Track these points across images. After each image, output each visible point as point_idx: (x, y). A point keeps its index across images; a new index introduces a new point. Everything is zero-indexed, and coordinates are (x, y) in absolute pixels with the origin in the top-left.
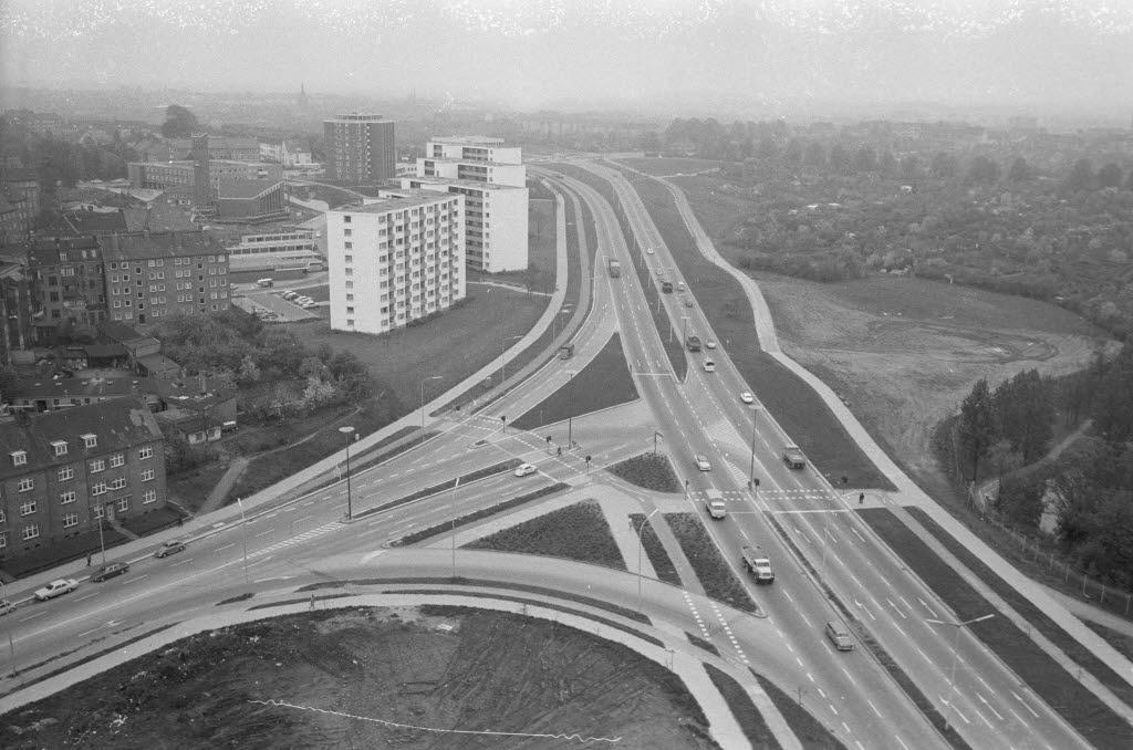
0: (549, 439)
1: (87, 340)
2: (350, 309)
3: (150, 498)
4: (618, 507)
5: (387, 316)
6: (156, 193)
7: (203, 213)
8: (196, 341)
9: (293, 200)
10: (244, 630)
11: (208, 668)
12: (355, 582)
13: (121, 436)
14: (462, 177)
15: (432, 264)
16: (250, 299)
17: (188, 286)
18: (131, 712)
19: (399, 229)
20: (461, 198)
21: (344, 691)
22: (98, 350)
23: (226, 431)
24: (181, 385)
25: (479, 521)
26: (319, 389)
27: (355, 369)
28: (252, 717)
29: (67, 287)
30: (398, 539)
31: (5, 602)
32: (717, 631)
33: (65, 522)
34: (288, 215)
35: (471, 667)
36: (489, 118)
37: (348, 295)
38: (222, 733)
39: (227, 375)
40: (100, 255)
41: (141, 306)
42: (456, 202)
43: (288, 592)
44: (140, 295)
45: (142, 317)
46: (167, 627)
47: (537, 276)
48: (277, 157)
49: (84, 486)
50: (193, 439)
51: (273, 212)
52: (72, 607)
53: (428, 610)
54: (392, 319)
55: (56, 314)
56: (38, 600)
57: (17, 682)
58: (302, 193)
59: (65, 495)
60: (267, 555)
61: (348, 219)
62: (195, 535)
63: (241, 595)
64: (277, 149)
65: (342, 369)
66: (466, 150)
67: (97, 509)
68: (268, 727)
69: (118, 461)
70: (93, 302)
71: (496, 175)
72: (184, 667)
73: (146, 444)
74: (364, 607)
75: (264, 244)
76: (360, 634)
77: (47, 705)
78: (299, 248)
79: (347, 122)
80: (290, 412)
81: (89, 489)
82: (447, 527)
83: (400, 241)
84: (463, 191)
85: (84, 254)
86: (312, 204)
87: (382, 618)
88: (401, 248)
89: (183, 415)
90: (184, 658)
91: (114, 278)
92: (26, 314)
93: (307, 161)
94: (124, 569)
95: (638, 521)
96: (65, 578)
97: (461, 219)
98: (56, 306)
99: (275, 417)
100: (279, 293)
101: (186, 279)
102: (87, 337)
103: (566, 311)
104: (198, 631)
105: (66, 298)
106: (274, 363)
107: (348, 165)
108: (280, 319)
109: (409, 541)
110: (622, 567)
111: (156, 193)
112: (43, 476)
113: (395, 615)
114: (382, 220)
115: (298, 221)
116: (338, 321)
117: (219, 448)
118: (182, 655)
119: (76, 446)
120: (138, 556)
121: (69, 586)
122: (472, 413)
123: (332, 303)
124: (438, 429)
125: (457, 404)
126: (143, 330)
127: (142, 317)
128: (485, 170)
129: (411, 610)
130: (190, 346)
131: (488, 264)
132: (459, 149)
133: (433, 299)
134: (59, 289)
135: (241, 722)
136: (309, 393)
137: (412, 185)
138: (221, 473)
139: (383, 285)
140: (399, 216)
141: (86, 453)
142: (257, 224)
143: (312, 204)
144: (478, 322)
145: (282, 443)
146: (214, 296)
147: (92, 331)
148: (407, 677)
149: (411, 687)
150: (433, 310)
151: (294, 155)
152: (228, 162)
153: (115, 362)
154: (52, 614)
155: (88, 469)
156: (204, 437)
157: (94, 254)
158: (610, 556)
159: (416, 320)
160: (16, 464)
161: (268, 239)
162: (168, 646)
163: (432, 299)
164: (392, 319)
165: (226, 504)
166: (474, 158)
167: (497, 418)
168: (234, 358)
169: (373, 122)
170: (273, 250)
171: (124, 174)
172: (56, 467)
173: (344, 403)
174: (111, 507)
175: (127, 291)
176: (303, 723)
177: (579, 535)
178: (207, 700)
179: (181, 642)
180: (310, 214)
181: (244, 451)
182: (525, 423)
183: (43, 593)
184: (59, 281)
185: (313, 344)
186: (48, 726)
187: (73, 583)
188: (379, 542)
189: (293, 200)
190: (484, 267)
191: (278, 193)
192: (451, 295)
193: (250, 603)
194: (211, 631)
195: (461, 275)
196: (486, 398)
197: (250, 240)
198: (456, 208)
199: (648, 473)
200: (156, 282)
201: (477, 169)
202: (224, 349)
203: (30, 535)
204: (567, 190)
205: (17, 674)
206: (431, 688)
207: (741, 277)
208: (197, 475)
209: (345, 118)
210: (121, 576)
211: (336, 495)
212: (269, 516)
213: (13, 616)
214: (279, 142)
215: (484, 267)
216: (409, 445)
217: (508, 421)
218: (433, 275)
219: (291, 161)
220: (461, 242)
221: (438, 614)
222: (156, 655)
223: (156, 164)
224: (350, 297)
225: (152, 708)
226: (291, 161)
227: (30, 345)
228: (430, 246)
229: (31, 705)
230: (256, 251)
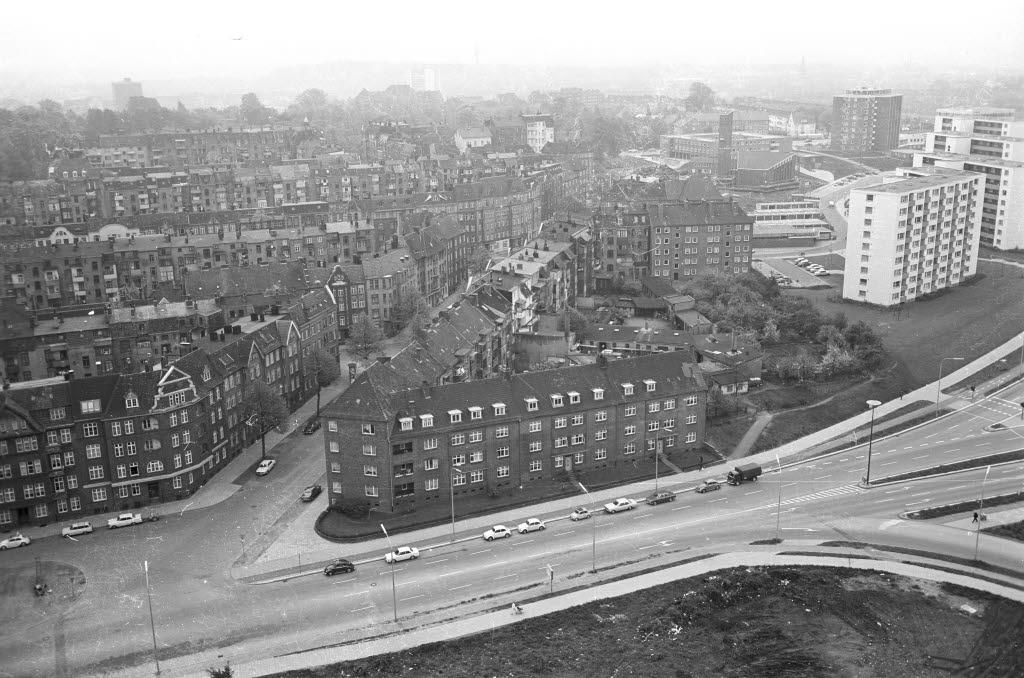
1: (633, 293)
2: (864, 281)
5: (899, 290)
6: (683, 162)
7: (723, 181)
8: (725, 302)
9: (803, 170)
10: (777, 572)
11: (747, 600)
12: (875, 547)
13: (675, 383)
14: (973, 152)
15: (946, 241)
16: (768, 263)
17: (717, 250)
18: (684, 625)
20: (982, 177)
21: (870, 649)
22: (643, 302)
23: (752, 385)
24: (714, 341)
25: (998, 507)
26: (837, 355)
27: (870, 339)
28: (786, 654)
29: (620, 247)
30: (916, 511)
31: (585, 509)
34: (798, 184)
35: (998, 655)
36: (990, 84)
37: (863, 268)
38: (761, 661)
39: (751, 334)
40: (647, 221)
42: (976, 181)
43: (812, 544)
45: (676, 275)
46: (710, 556)
48: (783, 128)
49: (643, 422)
50: (724, 390)
51: (785, 180)
52: (631, 522)
53: (949, 588)
54: (903, 292)
55: (610, 268)
57: (595, 578)
58: (809, 163)
59: (627, 428)
60: (792, 506)
61: (870, 198)
63: (771, 539)
64: (784, 120)
65: (857, 338)
66: (977, 124)
67: (651, 443)
68: (801, 666)
69: (670, 404)
70: (639, 260)
72: (726, 595)
74: (885, 573)
75: (775, 212)
76: (879, 595)
77: (620, 603)
78: (808, 217)
79: (857, 96)
80: (806, 374)
81: (646, 424)
83: (918, 220)
86: (818, 174)
87: (903, 586)
89: (718, 369)
90: (726, 587)
91: (658, 241)
92: (590, 268)
93: (811, 132)
94: (672, 498)
96: (627, 497)
97: (979, 199)
98: (610, 261)
99: (796, 379)
100: (792, 260)
101: (714, 244)
102: (633, 290)
104: (736, 565)
105: (619, 255)
106: (793, 326)
108: (794, 284)
109: (927, 515)
111: (683, 162)
112: (613, 411)
113: (916, 587)
114: (904, 199)
115: (804, 190)
116: (850, 291)
117: (746, 401)
118: (725, 584)
119: (640, 388)
120: (680, 488)
121: (412, 554)
122: (987, 394)
123: (847, 272)
124: (951, 406)
125: (970, 383)
126: (680, 287)
127: (676, 275)
128: (1000, 145)
129: (933, 585)
130: (720, 306)
131: (999, 241)
133: (944, 275)
134: (614, 247)
135: (777, 655)
136: (827, 359)
137: (925, 160)
138: (748, 425)
139: (899, 260)
140: (920, 196)
141: (648, 396)
142: (768, 192)
143: (818, 174)
145: (803, 403)
146: (737, 260)
147: (637, 285)
148: (930, 649)
149: (936, 661)
150: (943, 286)
151: (800, 126)
152: (744, 134)
153: (656, 314)
154: (618, 526)
155: (647, 409)
156: (734, 390)
157: (643, 219)
159: (925, 295)
160: (596, 398)
161: (779, 207)
162: (711, 573)
163: (944, 275)
164: (903, 292)
165: (753, 453)
166: (991, 132)
168: (758, 319)
170: (784, 217)
171: (656, 145)
172: (623, 405)
173: (858, 372)
176: (832, 671)
178: (746, 628)
179: (721, 572)
180: (817, 184)
181: (768, 407)
183: (611, 507)
184: (615, 241)
185: (827, 311)
186: (621, 621)
187: (633, 502)
188: (898, 512)
189: (803, 170)
190: (995, 244)
191: (790, 165)
192: (962, 272)
193: (778, 548)
194: (747, 567)
196: (1001, 380)
197: (764, 208)
198: (975, 187)
200: (691, 246)
202: (749, 310)
205: (595, 572)
206: (956, 667)
208: (729, 423)
210: (668, 504)
211: (852, 458)
213: (590, 521)
215: (995, 244)
216: (922, 419)
218: (946, 252)
219: (796, 132)
220: (977, 221)
221: (961, 595)
222: (702, 579)
223: (683, 137)
225: (702, 625)
226: (796, 132)
227: (591, 293)
228: (947, 224)
229: (608, 600)
230: (768, 218)
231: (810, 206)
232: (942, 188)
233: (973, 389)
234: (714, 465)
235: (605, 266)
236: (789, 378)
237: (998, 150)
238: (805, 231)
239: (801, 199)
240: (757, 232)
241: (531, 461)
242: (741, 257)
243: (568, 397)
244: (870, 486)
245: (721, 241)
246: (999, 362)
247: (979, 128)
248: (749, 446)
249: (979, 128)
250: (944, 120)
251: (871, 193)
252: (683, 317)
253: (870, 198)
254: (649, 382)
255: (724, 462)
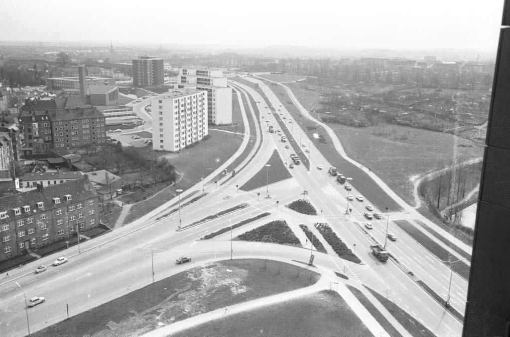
0: (259, 194)
3: (93, 222)
4: (294, 221)
19: (182, 106)
30: (203, 236)
32: (345, 269)
33: (59, 233)
41: (68, 141)
44: (94, 134)
47: (237, 126)
56: (54, 265)
59: (59, 221)
61: (160, 102)
62: (132, 230)
64: (108, 71)
69: (80, 205)
71: (215, 82)
73: (90, 199)
79: (143, 60)
82: (229, 229)
84: (206, 89)
85: (43, 119)
88: (183, 114)
95: (304, 228)
103: (252, 141)
107: (143, 81)
110: (301, 246)
125: (215, 181)
128: (209, 80)
131: (214, 121)
132: (195, 71)
141: (68, 203)
144: (216, 148)
146: (99, 136)
150: (190, 143)
158: (295, 242)
167: (234, 186)
169: (155, 59)
172: (56, 209)
174: (27, 242)
175: (61, 134)
177: (277, 233)
182: (247, 187)
183: (56, 262)
195: (206, 126)
199: (302, 207)
201: (206, 80)
203: (8, 251)
204: (241, 90)
207: (324, 125)
209: (142, 57)
212: (146, 228)
214: (110, 68)
217: (239, 187)
224: (161, 136)
226: (115, 77)
231: (129, 110)
232: (185, 98)
233: (216, 182)
234: (107, 233)
235: (28, 144)
236: (391, 105)
237: (208, 82)
238: (130, 121)
239: (125, 107)
240: (107, 123)
241: (4, 247)
242: (101, 135)
243: (23, 209)
244: (182, 230)
245: (90, 127)
246: (204, 178)
247: (198, 73)
248: (122, 222)
249: (198, 73)
250: (183, 70)
251: (160, 99)
252: (76, 165)
253: (160, 102)
254: (68, 196)
255: (112, 231)
